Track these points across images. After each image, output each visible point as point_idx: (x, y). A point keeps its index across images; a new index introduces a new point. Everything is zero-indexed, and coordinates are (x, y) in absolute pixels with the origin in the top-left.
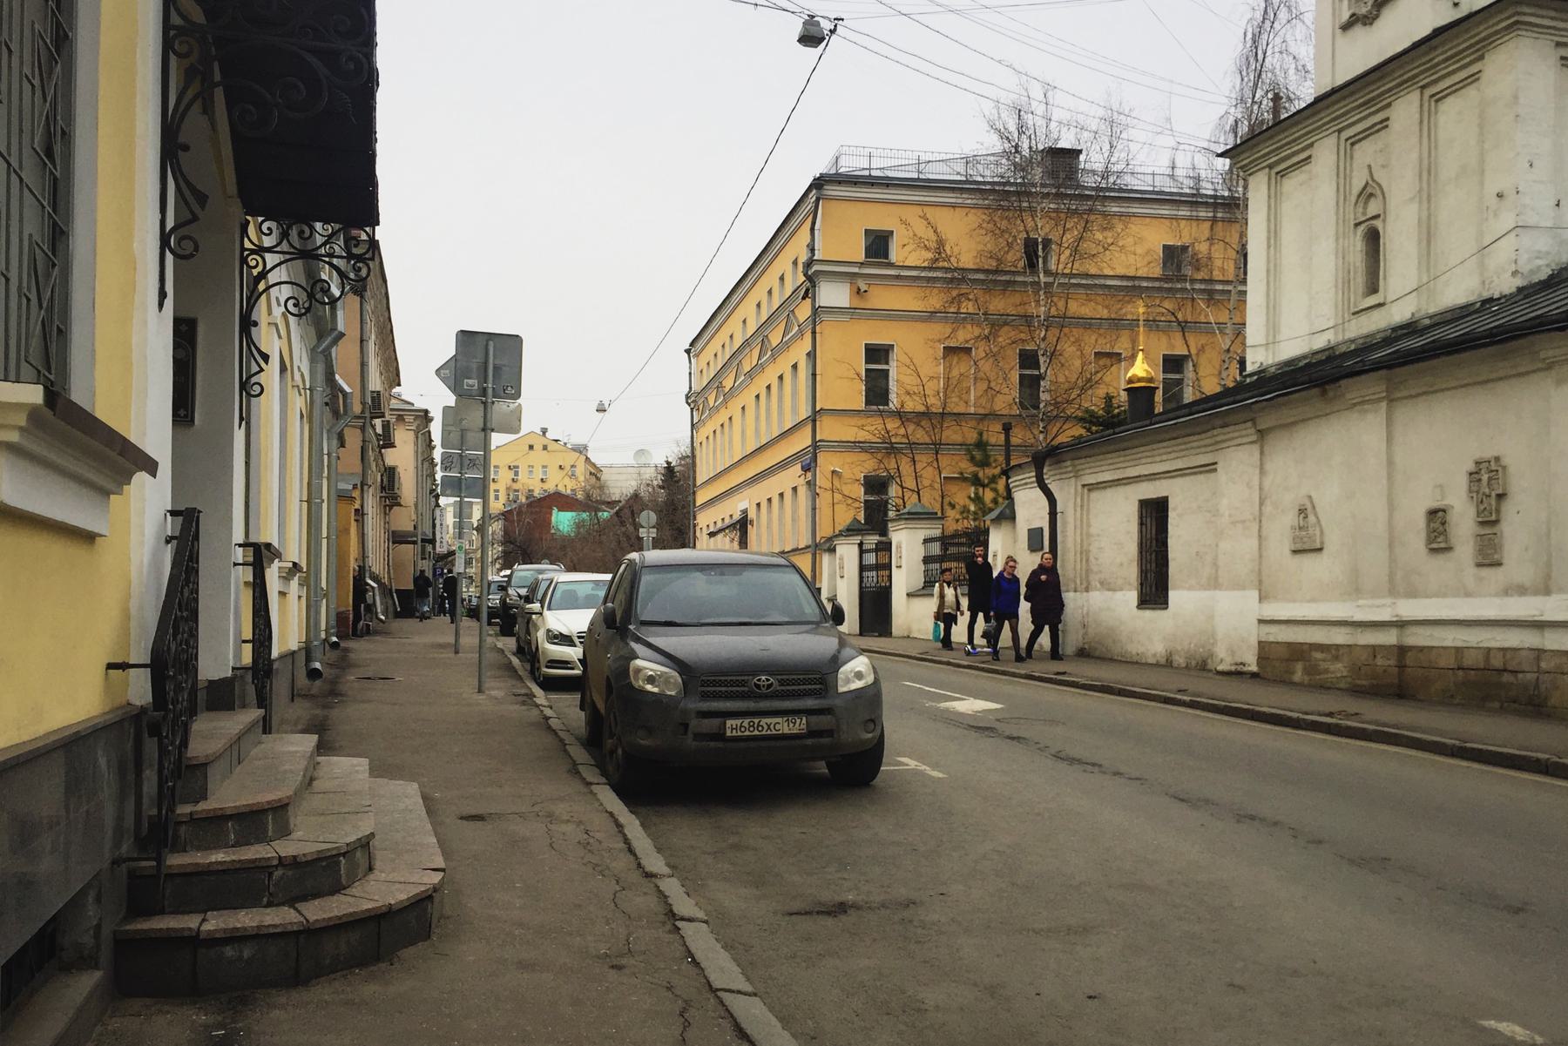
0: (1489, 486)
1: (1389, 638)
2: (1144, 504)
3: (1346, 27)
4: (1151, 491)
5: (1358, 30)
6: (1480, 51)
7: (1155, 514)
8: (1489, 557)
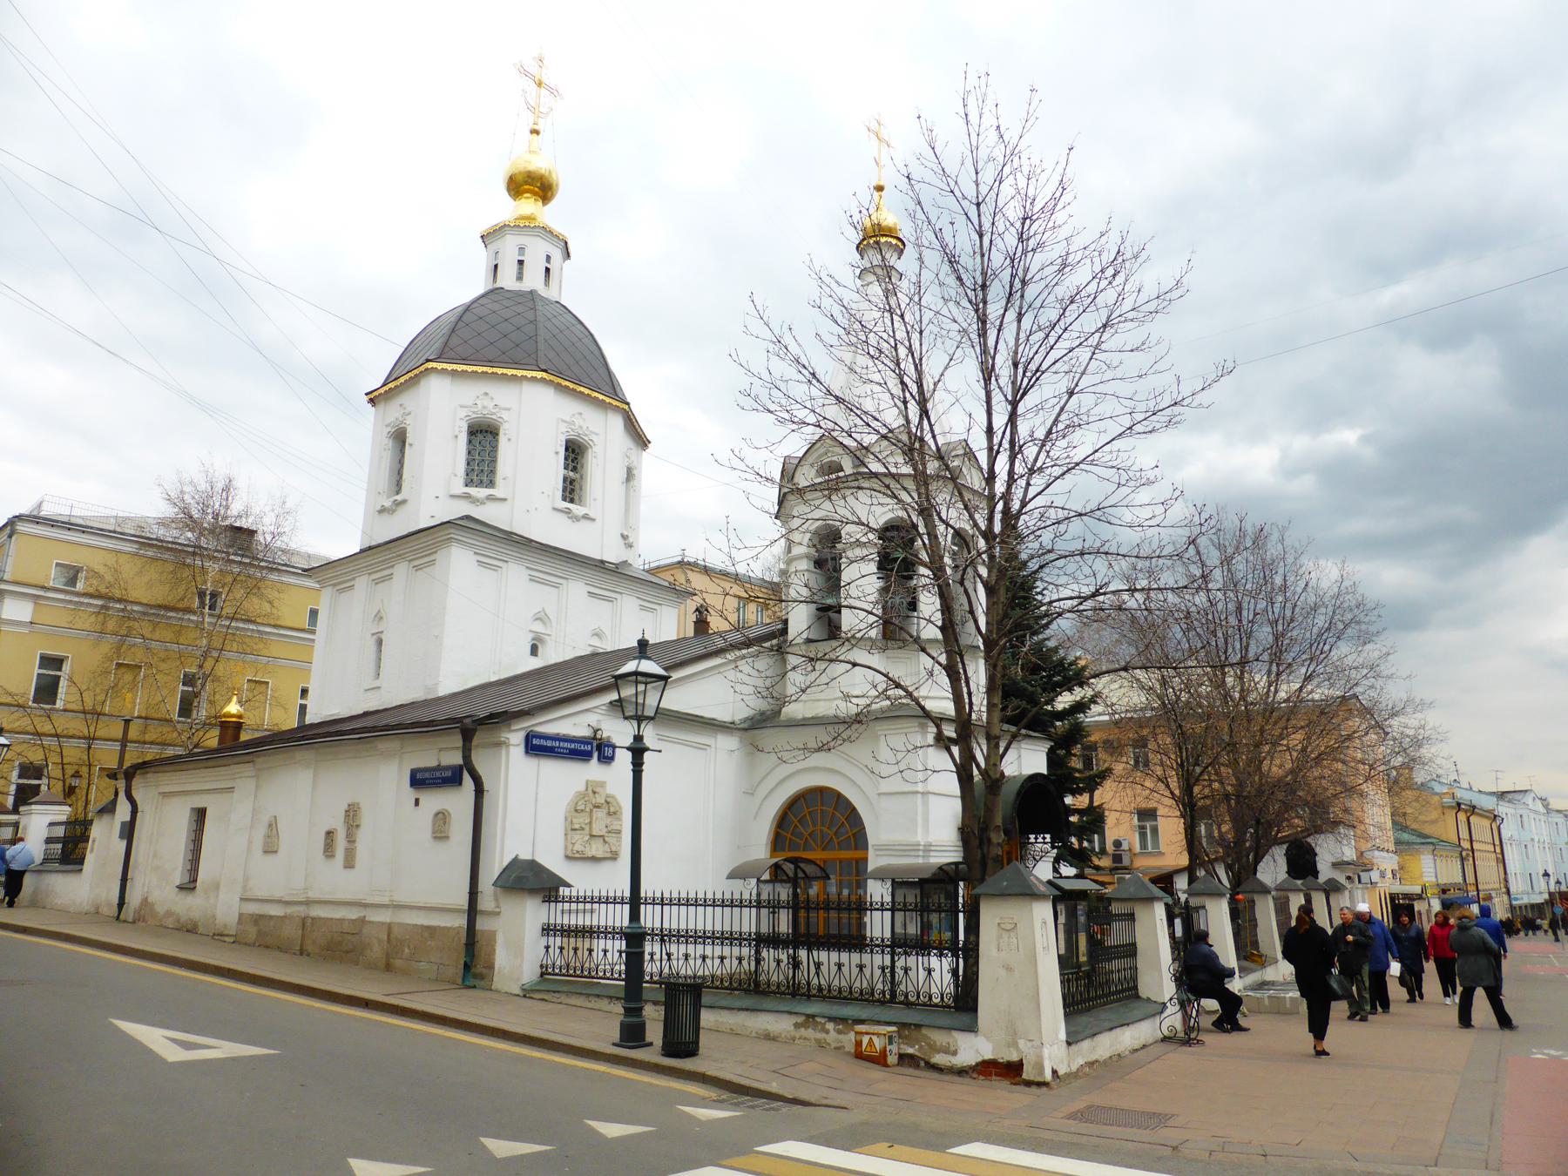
0: (352, 815)
1: (352, 914)
2: (352, 867)
3: (380, 512)
4: (199, 802)
5: (385, 516)
6: (433, 549)
7: (200, 814)
8: (349, 863)
